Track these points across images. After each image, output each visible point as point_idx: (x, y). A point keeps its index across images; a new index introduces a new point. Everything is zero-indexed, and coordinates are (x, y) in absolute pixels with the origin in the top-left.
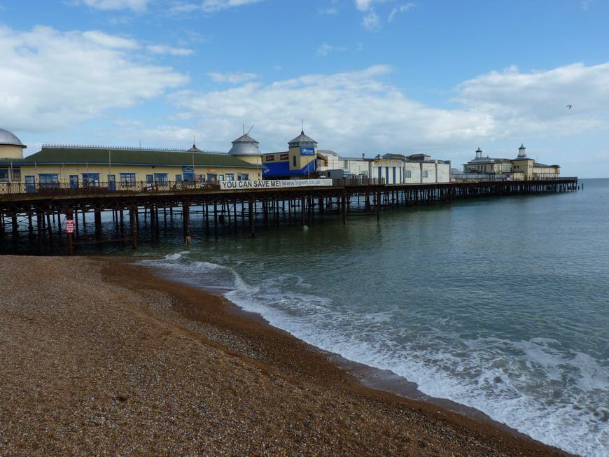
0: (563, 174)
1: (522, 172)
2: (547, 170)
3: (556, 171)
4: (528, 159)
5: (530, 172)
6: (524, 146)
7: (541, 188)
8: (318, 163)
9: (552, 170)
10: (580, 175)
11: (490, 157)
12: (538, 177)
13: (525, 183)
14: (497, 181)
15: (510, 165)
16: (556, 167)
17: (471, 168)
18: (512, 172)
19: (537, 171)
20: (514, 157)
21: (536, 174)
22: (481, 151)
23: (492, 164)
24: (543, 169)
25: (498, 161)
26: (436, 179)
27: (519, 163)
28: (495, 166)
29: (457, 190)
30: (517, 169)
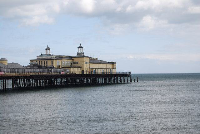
0: (120, 69)
1: (80, 67)
2: (104, 66)
3: (113, 66)
4: (84, 57)
5: (87, 67)
6: (82, 46)
7: (100, 81)
8: (79, 69)
9: (110, 66)
10: (134, 71)
11: (55, 52)
12: (95, 72)
13: (83, 76)
14: (54, 74)
15: (70, 61)
16: (113, 63)
17: (35, 64)
18: (72, 67)
19: (92, 66)
20: (74, 54)
21: (92, 69)
22: (82, 48)
23: (52, 60)
24: (100, 65)
25: (60, 58)
26: (127, 78)
27: (74, 60)
28: (55, 62)
29: (31, 80)
30: (76, 65)
